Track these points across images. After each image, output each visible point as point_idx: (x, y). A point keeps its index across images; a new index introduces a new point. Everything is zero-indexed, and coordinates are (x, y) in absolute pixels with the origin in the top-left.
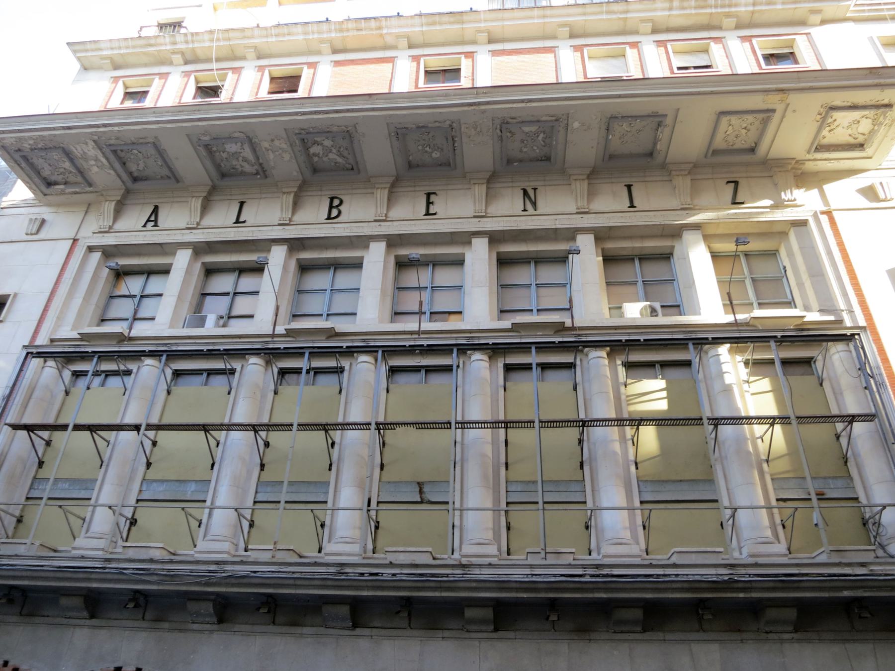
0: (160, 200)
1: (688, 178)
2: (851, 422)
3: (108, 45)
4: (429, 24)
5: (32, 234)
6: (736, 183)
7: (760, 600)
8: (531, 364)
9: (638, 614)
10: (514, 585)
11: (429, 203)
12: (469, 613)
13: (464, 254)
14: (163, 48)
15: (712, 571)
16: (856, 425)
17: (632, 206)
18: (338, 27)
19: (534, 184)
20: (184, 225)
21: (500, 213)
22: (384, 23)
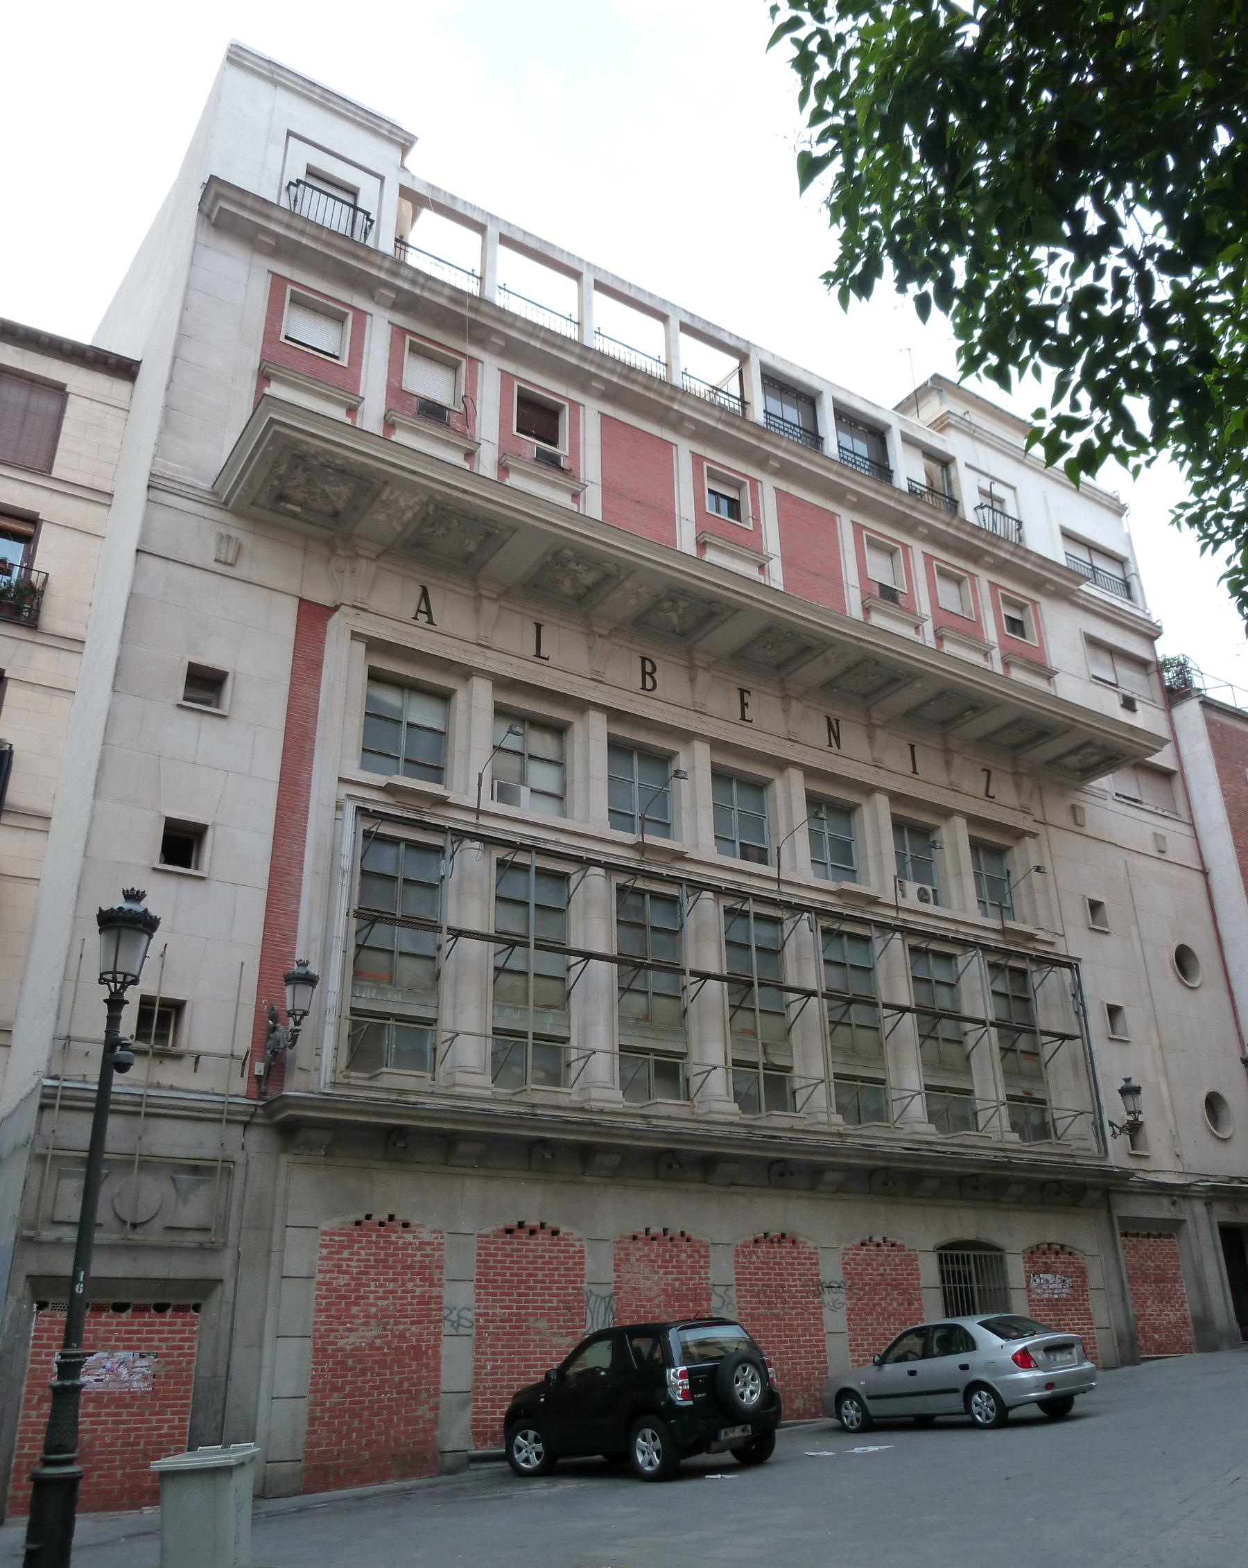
0: (432, 580)
1: (373, 565)
2: (373, 923)
3: (410, 275)
4: (725, 423)
5: (225, 563)
6: (989, 772)
7: (823, 1163)
8: (529, 866)
9: (616, 1160)
10: (627, 1132)
11: (744, 705)
12: (463, 1148)
13: (454, 691)
14: (374, 272)
15: (992, 1153)
16: (853, 1008)
17: (915, 772)
18: (625, 372)
19: (839, 714)
20: (472, 638)
21: (385, 610)
22: (679, 396)
